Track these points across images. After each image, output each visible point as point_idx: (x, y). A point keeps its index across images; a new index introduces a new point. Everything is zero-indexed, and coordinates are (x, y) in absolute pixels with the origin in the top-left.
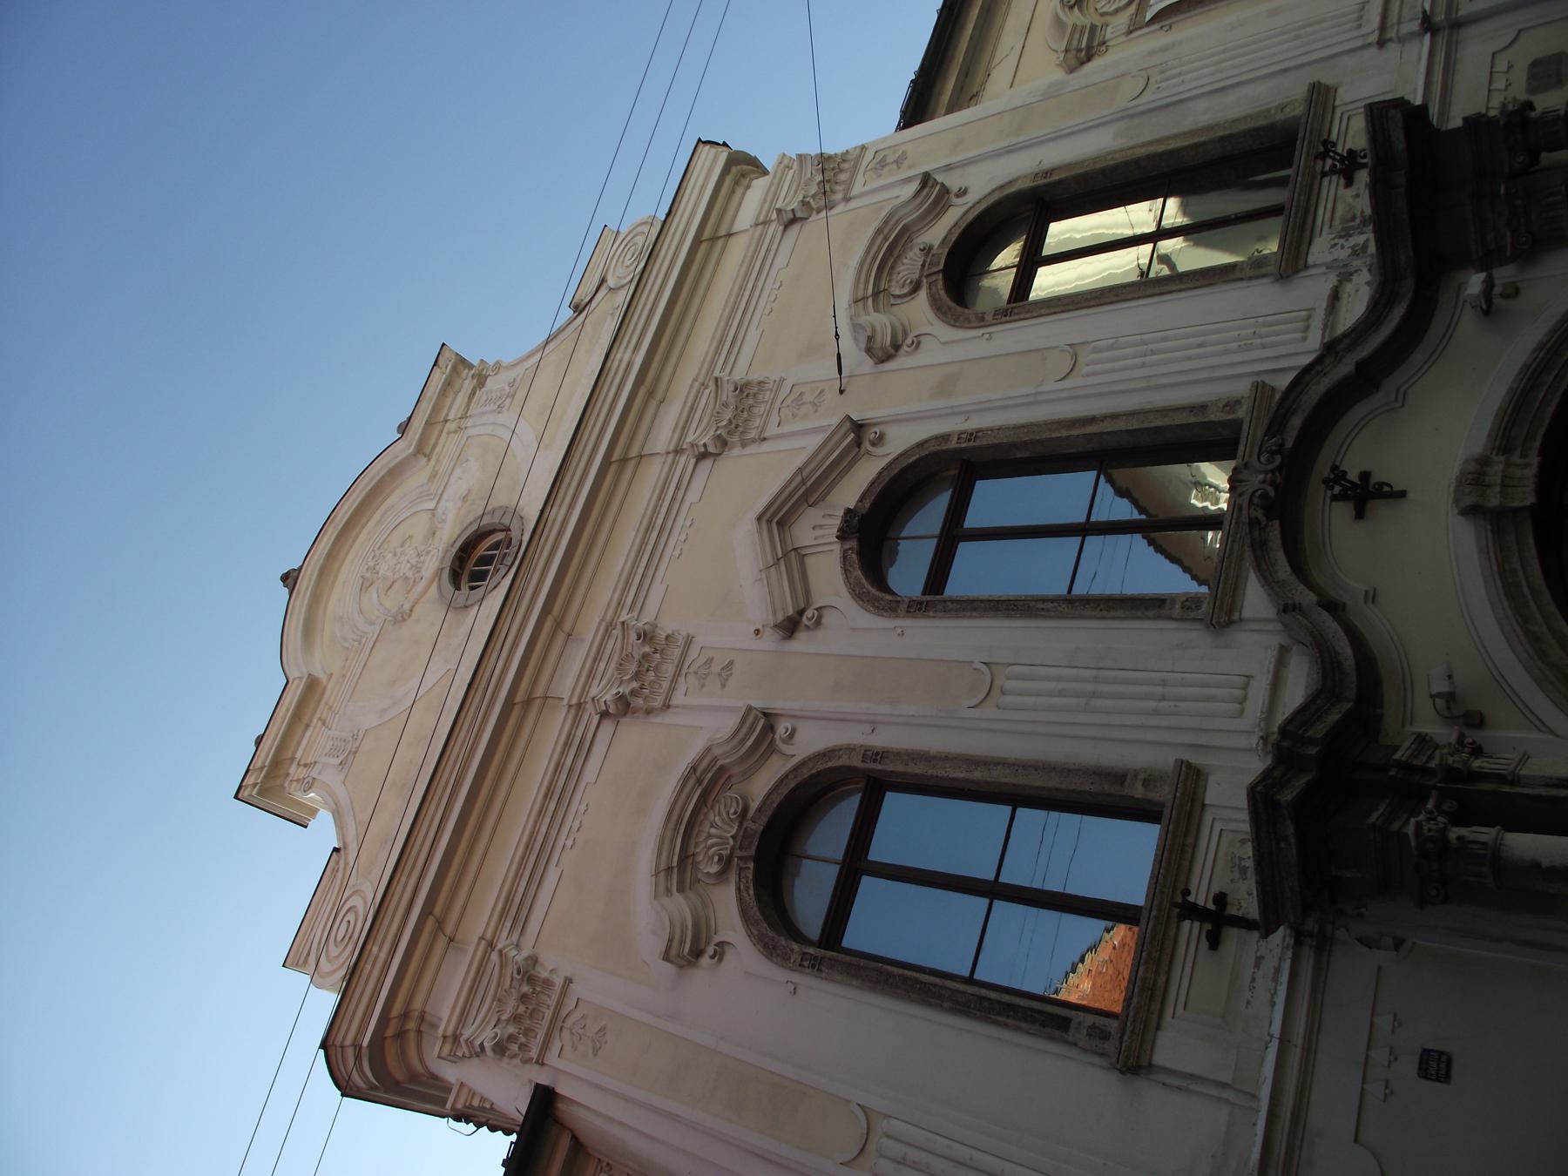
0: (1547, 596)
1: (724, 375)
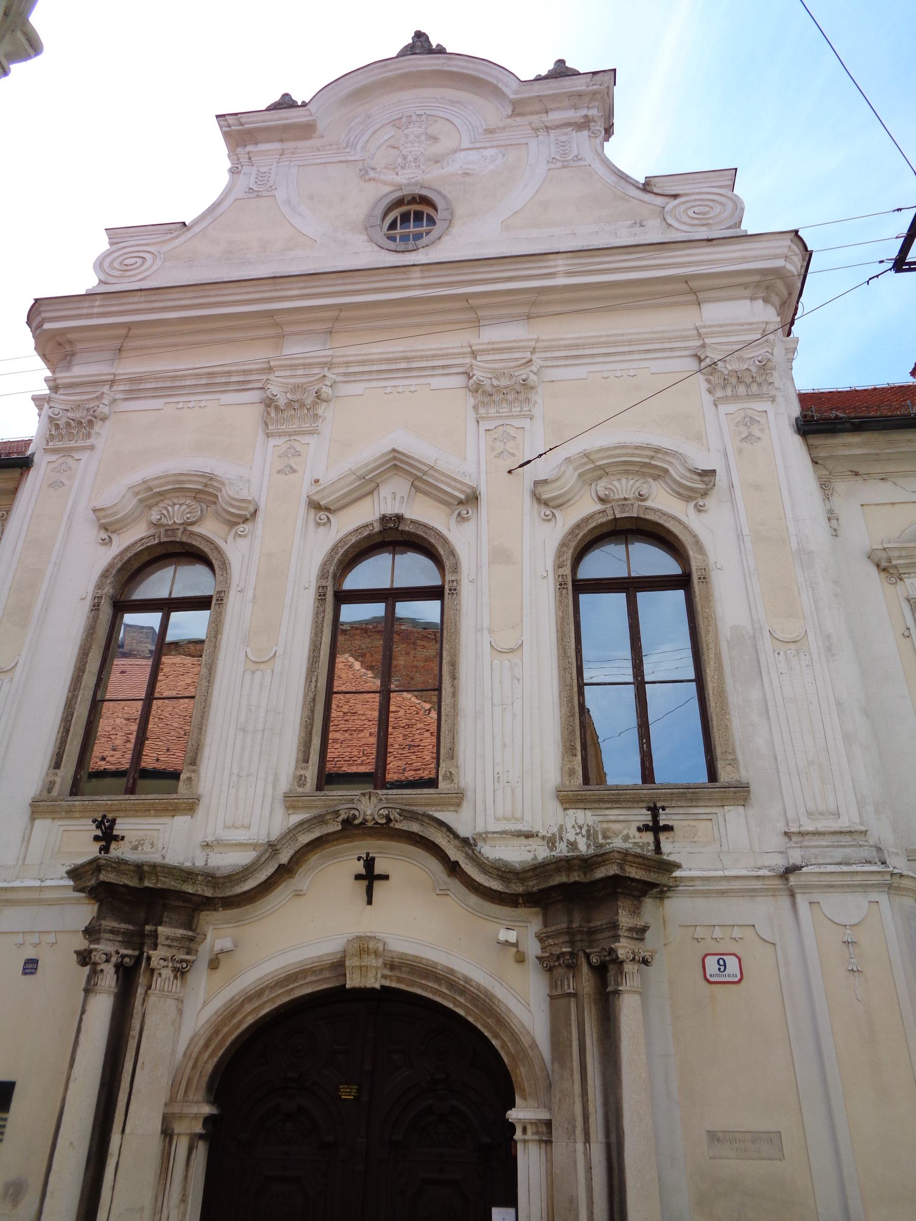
0: (286, 999)
1: (538, 362)
